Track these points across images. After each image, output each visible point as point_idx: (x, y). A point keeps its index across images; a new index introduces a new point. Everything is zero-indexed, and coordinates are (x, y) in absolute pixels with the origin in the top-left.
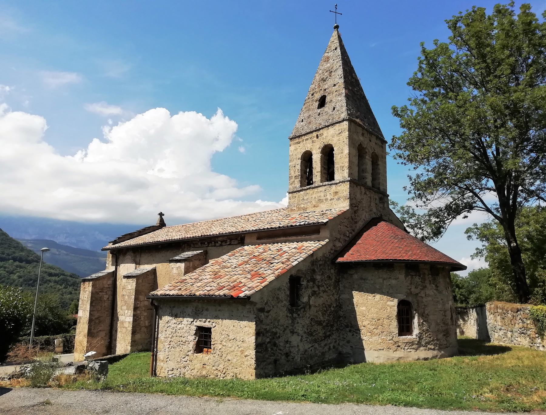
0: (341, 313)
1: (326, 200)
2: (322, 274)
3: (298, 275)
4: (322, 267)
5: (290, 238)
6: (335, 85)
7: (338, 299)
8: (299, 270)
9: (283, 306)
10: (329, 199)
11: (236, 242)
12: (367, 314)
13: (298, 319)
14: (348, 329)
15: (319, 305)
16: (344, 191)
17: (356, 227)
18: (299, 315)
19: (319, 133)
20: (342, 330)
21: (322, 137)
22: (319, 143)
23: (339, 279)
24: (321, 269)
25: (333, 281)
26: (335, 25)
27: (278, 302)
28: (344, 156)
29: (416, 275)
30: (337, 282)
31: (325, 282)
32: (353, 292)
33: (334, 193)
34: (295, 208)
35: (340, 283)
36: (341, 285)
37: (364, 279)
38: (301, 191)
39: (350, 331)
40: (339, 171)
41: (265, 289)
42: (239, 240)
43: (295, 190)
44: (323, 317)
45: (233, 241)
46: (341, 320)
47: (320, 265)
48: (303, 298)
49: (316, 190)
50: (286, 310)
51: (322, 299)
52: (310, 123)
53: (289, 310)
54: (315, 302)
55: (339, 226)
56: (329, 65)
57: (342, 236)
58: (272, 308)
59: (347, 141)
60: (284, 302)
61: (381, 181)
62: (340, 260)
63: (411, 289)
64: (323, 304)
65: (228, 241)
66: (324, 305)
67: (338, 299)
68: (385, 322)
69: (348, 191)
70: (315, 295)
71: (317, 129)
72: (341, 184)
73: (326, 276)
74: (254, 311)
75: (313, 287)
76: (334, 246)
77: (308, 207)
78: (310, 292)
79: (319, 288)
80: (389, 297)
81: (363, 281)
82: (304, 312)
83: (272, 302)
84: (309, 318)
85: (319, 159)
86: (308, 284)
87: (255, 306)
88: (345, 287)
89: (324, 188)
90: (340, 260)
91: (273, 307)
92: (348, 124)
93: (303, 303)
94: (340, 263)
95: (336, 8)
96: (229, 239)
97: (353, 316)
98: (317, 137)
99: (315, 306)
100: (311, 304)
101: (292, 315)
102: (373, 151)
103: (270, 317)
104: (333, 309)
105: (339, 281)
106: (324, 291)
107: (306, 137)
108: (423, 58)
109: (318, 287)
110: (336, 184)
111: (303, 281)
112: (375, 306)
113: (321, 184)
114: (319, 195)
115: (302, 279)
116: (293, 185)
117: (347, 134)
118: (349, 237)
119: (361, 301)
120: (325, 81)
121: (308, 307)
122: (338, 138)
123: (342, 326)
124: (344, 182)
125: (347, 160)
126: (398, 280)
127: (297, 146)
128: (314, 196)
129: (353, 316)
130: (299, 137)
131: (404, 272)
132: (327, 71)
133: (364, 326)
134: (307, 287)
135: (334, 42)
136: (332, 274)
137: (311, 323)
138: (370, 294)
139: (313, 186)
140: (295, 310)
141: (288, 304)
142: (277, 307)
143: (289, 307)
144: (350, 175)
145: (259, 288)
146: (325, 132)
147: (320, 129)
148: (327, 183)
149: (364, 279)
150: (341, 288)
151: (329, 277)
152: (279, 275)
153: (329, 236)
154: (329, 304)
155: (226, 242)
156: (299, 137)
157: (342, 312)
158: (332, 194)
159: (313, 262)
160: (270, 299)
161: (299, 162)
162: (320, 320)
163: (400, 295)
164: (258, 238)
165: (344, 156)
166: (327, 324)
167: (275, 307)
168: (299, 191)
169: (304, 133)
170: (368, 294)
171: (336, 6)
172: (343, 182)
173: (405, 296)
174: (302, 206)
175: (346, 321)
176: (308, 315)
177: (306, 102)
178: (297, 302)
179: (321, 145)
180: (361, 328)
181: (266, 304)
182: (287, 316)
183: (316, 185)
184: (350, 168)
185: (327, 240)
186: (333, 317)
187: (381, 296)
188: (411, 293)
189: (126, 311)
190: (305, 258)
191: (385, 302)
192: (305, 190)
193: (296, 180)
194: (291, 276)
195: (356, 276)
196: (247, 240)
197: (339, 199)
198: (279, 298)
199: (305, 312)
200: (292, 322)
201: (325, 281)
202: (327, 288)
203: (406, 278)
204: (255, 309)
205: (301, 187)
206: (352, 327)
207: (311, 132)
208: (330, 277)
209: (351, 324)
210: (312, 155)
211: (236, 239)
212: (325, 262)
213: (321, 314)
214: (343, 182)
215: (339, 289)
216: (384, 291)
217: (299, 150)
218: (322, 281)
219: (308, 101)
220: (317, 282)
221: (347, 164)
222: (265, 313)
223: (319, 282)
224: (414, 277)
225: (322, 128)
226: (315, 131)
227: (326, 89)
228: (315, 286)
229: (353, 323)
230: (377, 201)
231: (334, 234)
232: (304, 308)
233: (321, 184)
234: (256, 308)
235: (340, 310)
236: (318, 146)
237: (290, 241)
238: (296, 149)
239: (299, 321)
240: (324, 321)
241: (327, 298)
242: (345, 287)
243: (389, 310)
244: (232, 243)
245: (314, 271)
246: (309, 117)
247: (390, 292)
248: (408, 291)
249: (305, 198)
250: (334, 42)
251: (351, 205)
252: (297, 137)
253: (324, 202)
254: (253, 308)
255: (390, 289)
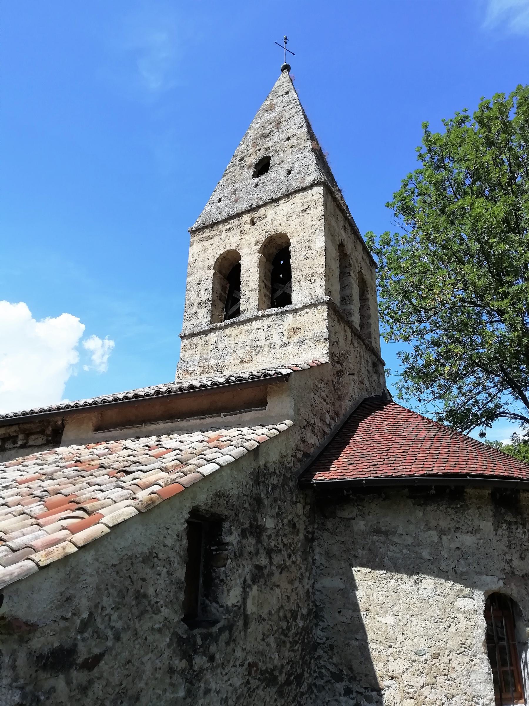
0: (319, 633)
1: (272, 346)
2: (278, 515)
3: (216, 510)
4: (277, 493)
5: (184, 423)
6: (288, 139)
7: (310, 590)
8: (219, 495)
9: (160, 631)
10: (278, 342)
11: (41, 440)
12: (401, 638)
13: (208, 676)
14: (340, 686)
15: (270, 613)
16: (315, 326)
17: (340, 406)
18: (212, 658)
19: (255, 215)
20: (321, 689)
21: (264, 221)
22: (256, 233)
23: (313, 533)
24: (276, 500)
25: (301, 536)
26: (285, 64)
27: (140, 616)
28: (314, 253)
29: (516, 523)
30: (310, 540)
31: (285, 540)
32: (355, 570)
33: (289, 330)
34: (196, 368)
35: (315, 543)
36: (317, 550)
37: (386, 533)
38: (211, 331)
39: (348, 692)
40: (303, 284)
41: (89, 556)
42: (47, 436)
43: (198, 330)
44: (279, 652)
45: (33, 437)
46: (319, 657)
47: (274, 487)
48: (229, 591)
49: (246, 327)
50: (169, 646)
51: (278, 591)
52: (236, 201)
53: (180, 640)
54: (260, 605)
55: (312, 394)
56: (274, 114)
57: (317, 421)
58: (110, 643)
59: (321, 224)
60: (165, 611)
61: (372, 330)
62: (320, 477)
63: (511, 560)
64: (279, 610)
65: (21, 436)
66: (282, 614)
67: (310, 590)
68: (454, 664)
69: (325, 324)
70: (262, 581)
71: (254, 206)
72: (307, 310)
73: (286, 521)
74: (14, 667)
75: (257, 553)
76: (304, 441)
77: (226, 363)
78: (247, 569)
79: (271, 558)
80: (459, 586)
81: (382, 538)
82: (227, 644)
83: (115, 616)
84: (241, 665)
85: (257, 264)
86: (244, 541)
87: (23, 641)
88: (328, 555)
89: (266, 321)
90: (320, 477)
91: (117, 638)
92: (322, 192)
93: (228, 610)
94: (322, 485)
95: (286, 43)
96: (23, 431)
97: (354, 643)
98: (253, 223)
99: (261, 619)
100: (249, 612)
101: (190, 661)
102: (360, 269)
103: (98, 688)
104: (301, 623)
105: (313, 540)
106: (282, 568)
107: (227, 226)
108: (424, 150)
109: (269, 552)
110: (296, 310)
111: (230, 533)
112: (422, 612)
113: (260, 313)
114: (253, 336)
115: (226, 525)
116: (194, 321)
117: (320, 210)
118: (329, 425)
119: (377, 598)
120: (267, 136)
121: (241, 623)
122: (300, 220)
123: (321, 676)
124: (315, 305)
125: (322, 260)
126: (478, 536)
127: (207, 243)
128: (240, 341)
129: (354, 643)
130: (212, 226)
131: (491, 513)
132: (271, 123)
133: (392, 678)
134: (239, 555)
135: (284, 86)
136: (298, 516)
137: (248, 682)
138: (405, 577)
139: (241, 318)
140: (199, 642)
141: (176, 618)
142: (136, 634)
143: (182, 629)
144: (328, 292)
145: (57, 553)
146: (270, 212)
147: (259, 207)
148: (273, 310)
149: (386, 533)
150: (320, 560)
151: (293, 525)
152: (153, 501)
153: (291, 412)
154: (294, 607)
155: (14, 439)
156: (212, 226)
157: (323, 630)
158: (285, 333)
159: (258, 473)
160: (106, 601)
161: (210, 273)
162: (270, 666)
163: (488, 579)
164: (98, 429)
165: (314, 253)
166: (289, 674)
167: (125, 637)
168: (205, 333)
169: (223, 218)
170: (399, 576)
171: (286, 39)
172: (313, 306)
173: (501, 583)
174: (213, 362)
175: (335, 660)
176: (239, 654)
177: (228, 171)
178: (205, 607)
179: (261, 236)
180: (385, 683)
181: (85, 626)
182: (171, 671)
183: (248, 316)
184: (327, 277)
185: (289, 422)
186: (303, 650)
187: (437, 580)
188: (513, 573)
190: (238, 456)
191: (450, 598)
192: (221, 328)
193: (200, 311)
194: (195, 512)
195: (360, 525)
196: (68, 433)
197: (302, 342)
198: (145, 596)
199: (232, 645)
200: (189, 693)
201: (285, 535)
202: (290, 556)
203: (496, 530)
204: (22, 660)
205: (211, 323)
206: (352, 679)
207: (239, 215)
208: (294, 526)
209: (351, 669)
210: (239, 258)
211: (42, 432)
212: (285, 483)
213: (274, 645)
214: (313, 306)
215: (314, 560)
216: (444, 567)
217: (210, 251)
218: (277, 535)
219: (232, 169)
220: (265, 538)
221: (321, 270)
222: (74, 673)
223: (270, 537)
224: (514, 527)
225: (265, 205)
226: (248, 211)
227: (269, 148)
228: (261, 551)
229: (355, 665)
230: (370, 368)
231: (303, 410)
232: (230, 627)
233: (260, 313)
234: (30, 654)
235: (316, 625)
236: (254, 240)
237: (182, 431)
238: (203, 251)
239: (213, 686)
240: (282, 666)
241: (289, 587)
242: (328, 555)
243: (462, 626)
244: (31, 443)
245: (259, 501)
246: (234, 192)
247: (462, 568)
248: (507, 566)
249: (220, 345)
250: (284, 86)
251: (332, 355)
252: (207, 227)
253: (267, 350)
254: (13, 654)
255: (462, 561)
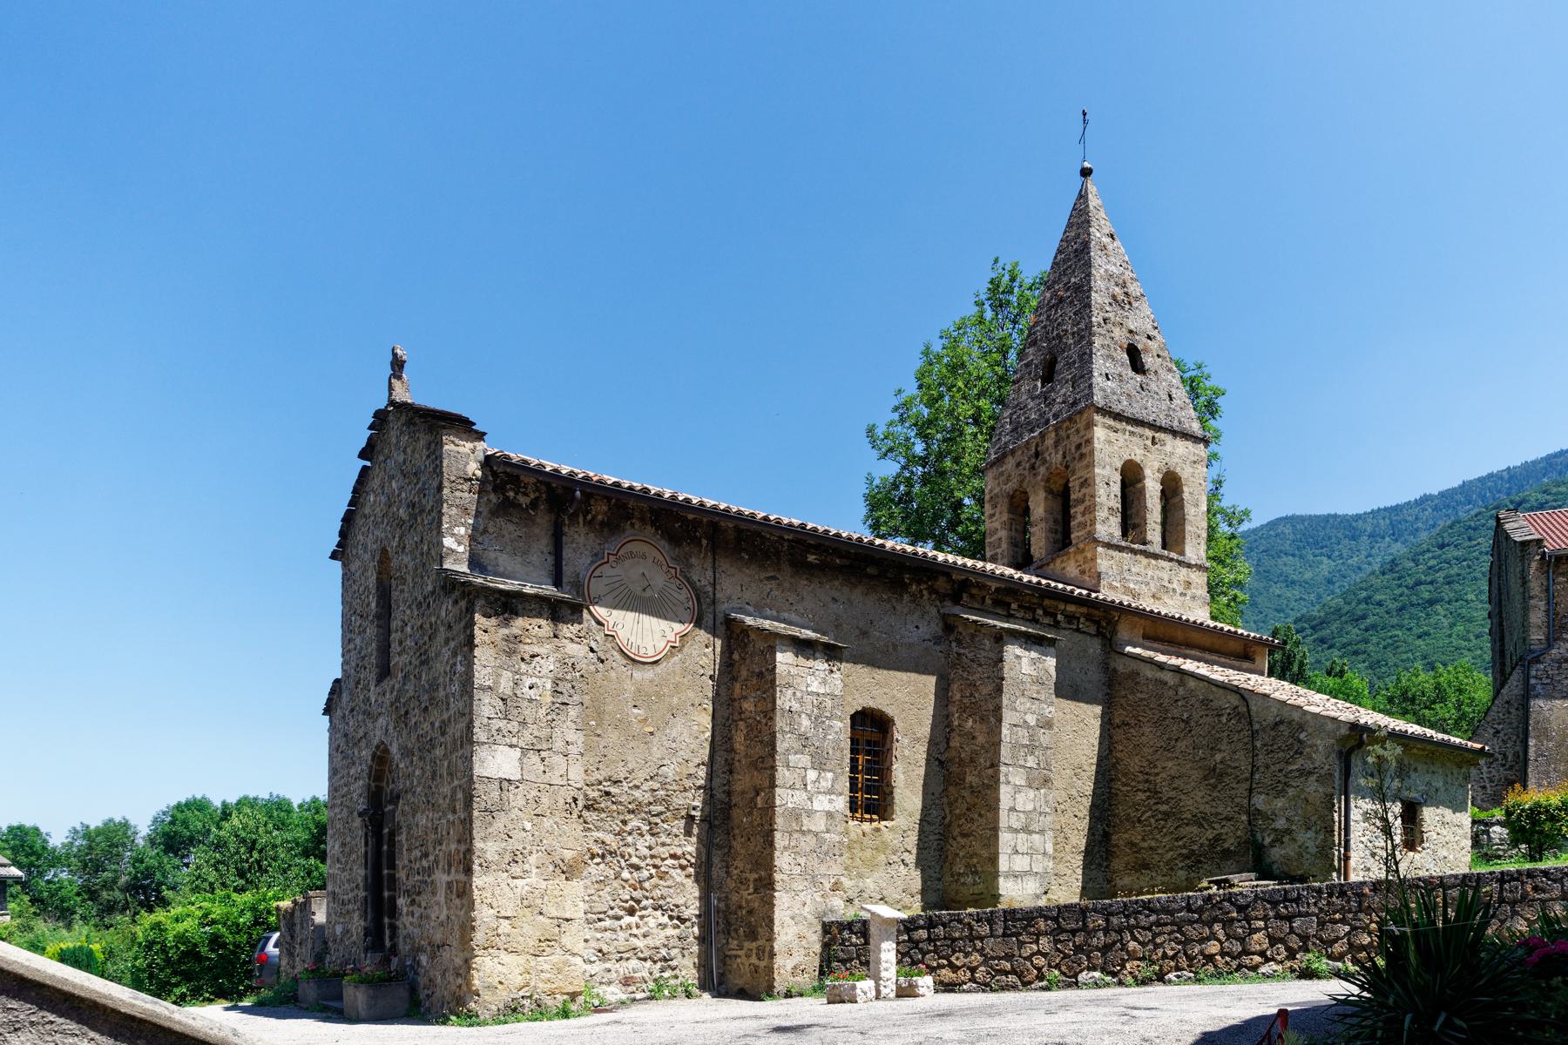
189: (812, 775)
